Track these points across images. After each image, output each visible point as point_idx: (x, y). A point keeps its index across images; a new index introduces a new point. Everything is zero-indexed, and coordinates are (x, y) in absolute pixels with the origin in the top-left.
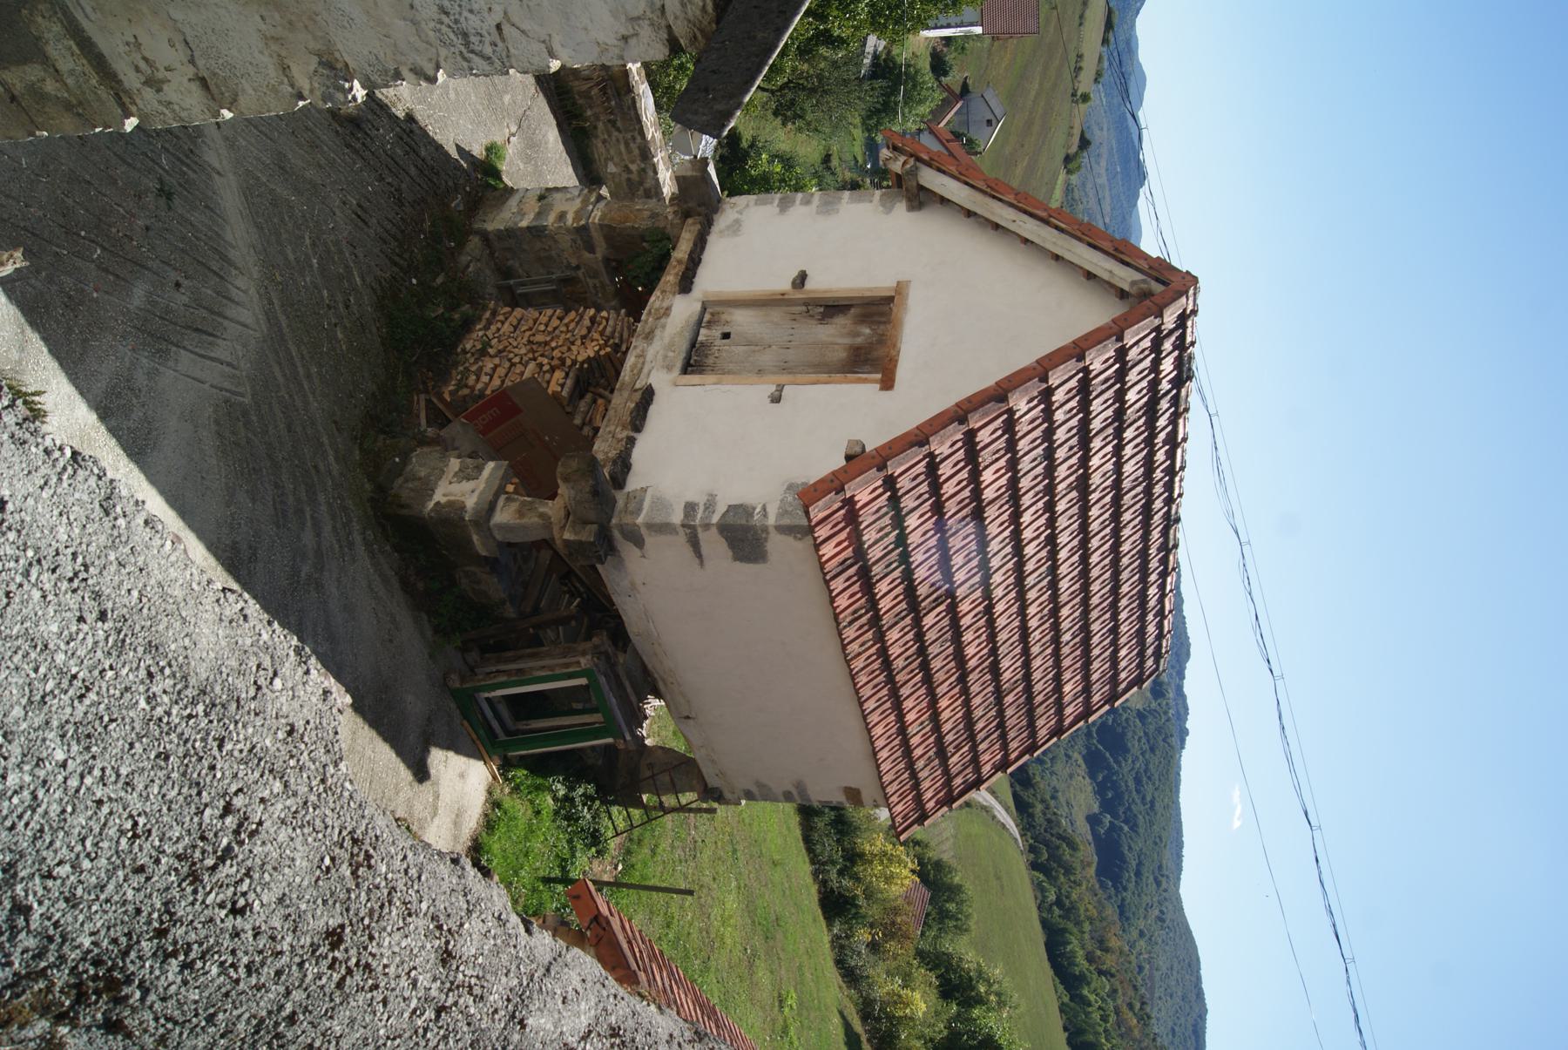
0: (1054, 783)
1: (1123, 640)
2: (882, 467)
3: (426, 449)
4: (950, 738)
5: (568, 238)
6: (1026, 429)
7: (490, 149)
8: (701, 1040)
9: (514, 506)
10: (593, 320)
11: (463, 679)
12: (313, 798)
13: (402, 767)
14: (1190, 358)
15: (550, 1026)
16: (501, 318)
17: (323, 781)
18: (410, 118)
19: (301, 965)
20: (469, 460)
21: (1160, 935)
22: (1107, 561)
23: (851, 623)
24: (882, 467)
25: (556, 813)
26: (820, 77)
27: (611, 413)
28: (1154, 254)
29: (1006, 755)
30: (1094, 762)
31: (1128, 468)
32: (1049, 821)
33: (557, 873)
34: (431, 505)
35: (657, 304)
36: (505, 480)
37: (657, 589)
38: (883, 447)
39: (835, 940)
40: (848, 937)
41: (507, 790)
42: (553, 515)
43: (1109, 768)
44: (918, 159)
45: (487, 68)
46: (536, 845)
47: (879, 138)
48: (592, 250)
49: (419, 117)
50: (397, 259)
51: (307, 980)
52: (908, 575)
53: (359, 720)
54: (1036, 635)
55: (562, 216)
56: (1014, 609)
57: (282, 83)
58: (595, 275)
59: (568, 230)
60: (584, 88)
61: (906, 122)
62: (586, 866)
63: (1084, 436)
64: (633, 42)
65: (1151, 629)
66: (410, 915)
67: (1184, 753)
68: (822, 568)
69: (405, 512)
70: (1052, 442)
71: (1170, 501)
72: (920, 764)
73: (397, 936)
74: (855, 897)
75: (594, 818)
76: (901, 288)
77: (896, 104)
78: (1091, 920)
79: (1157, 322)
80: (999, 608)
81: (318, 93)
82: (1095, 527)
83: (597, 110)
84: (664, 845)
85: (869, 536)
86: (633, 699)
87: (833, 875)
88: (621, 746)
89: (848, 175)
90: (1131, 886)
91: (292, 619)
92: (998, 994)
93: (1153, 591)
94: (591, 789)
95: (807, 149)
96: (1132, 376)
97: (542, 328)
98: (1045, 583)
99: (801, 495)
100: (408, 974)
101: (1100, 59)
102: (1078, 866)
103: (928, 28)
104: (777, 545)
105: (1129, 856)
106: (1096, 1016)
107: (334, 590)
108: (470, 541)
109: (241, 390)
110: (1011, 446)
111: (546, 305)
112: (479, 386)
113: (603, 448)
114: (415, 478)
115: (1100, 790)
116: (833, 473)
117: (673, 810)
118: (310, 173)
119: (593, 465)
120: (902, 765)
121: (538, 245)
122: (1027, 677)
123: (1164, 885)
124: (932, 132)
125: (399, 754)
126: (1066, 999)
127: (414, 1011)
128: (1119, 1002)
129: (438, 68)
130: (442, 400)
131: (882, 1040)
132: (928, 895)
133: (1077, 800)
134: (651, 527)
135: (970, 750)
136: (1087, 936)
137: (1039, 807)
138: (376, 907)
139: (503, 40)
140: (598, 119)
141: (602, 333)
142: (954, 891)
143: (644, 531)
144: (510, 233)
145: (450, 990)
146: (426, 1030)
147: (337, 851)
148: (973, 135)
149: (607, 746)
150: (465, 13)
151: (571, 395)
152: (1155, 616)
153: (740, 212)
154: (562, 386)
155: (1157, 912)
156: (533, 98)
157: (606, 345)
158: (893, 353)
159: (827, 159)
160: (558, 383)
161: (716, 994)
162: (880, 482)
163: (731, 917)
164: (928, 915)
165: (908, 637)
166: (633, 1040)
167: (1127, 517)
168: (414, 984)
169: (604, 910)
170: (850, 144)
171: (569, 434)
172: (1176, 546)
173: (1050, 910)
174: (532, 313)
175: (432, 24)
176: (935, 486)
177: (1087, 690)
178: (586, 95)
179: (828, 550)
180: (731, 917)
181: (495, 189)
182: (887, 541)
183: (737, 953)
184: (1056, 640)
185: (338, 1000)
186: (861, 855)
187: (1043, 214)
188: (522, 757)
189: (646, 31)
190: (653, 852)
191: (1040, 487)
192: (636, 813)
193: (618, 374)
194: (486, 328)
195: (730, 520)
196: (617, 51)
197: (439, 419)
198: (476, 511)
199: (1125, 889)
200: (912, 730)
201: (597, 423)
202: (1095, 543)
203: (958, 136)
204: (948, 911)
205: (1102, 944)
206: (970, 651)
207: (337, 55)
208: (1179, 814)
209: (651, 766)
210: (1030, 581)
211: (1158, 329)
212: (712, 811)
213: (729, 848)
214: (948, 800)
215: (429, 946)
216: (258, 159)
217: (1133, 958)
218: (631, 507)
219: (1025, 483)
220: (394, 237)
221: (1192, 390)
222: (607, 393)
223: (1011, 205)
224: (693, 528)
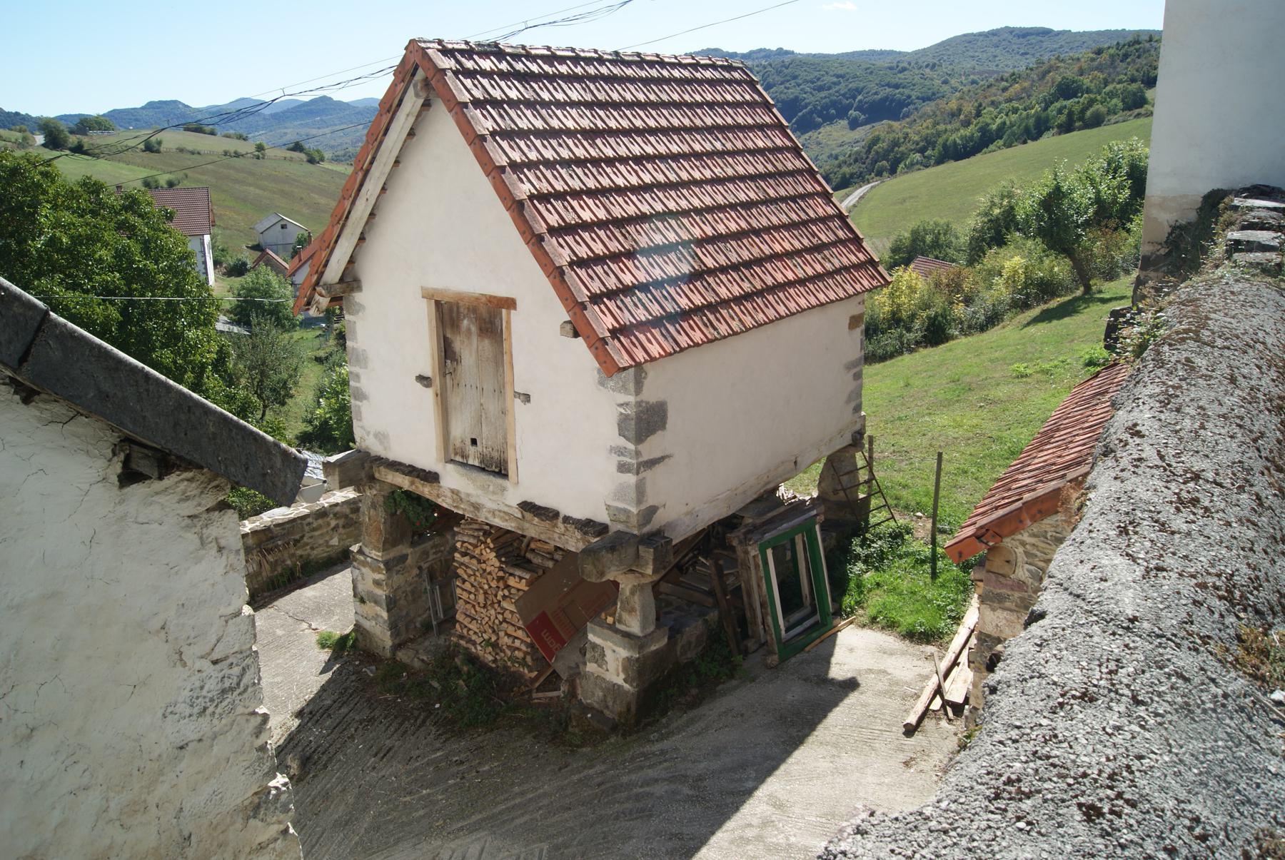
0: (824, 157)
1: (719, 98)
2: (583, 306)
3: (579, 691)
4: (806, 242)
5: (395, 578)
6: (545, 184)
7: (323, 646)
8: (1112, 451)
9: (625, 616)
10: (464, 554)
11: (771, 653)
12: (964, 842)
13: (847, 701)
14: (479, 45)
15: (1130, 593)
16: (465, 631)
17: (945, 832)
18: (299, 714)
19: (1123, 847)
20: (588, 656)
21: (946, 68)
22: (653, 113)
23: (715, 329)
24: (583, 306)
25: (877, 569)
26: (251, 368)
27: (543, 537)
28: (391, 78)
29: (818, 194)
30: (805, 125)
31: (575, 96)
32: (856, 160)
33: (927, 567)
34: (627, 686)
35: (449, 501)
36: (603, 625)
37: (690, 494)
38: (566, 306)
39: (965, 333)
40: (961, 323)
41: (861, 612)
42: (632, 584)
43: (811, 112)
44: (317, 283)
45: (252, 670)
46: (905, 585)
47: (300, 317)
48: (403, 558)
49: (299, 707)
50: (419, 722)
51: (1136, 839)
52: (673, 281)
53: (811, 739)
54: (718, 171)
55: (377, 583)
56: (697, 190)
57: (274, 849)
58: (425, 553)
59: (388, 578)
60: (267, 566)
61: (285, 294)
62: (919, 544)
63: (548, 134)
64: (223, 543)
65: (708, 74)
66: (1056, 736)
67: (797, 51)
68: (670, 354)
69: (633, 709)
70: (555, 162)
71: (601, 61)
72: (829, 266)
73: (1078, 748)
74: (929, 317)
75: (880, 539)
76: (428, 295)
77: (271, 304)
78: (936, 124)
79: (449, 74)
80: (696, 203)
81: (282, 816)
82: (625, 124)
83: (286, 555)
84: (898, 477)
85: (642, 315)
86: (782, 509)
87: (911, 336)
88: (822, 518)
89: (332, 342)
90: (907, 92)
91: (729, 800)
92: (1002, 197)
93: (676, 73)
94: (856, 541)
95: (311, 377)
96: (497, 94)
97: (472, 596)
98: (673, 165)
99: (610, 376)
100: (1110, 735)
101: (227, 136)
102: (891, 136)
103: (207, 279)
104: (651, 393)
105: (882, 95)
106: (1014, 117)
107: (702, 765)
108: (656, 652)
109: (537, 853)
110: (560, 196)
111: (453, 594)
112: (524, 648)
113: (574, 542)
114: (604, 700)
115: (829, 119)
116: (590, 347)
117: (871, 471)
118: (350, 799)
119: (589, 552)
120: (830, 281)
121: (402, 602)
122: (753, 178)
123: (905, 65)
124: (293, 274)
125: (836, 705)
126: (1001, 142)
127: (1142, 727)
128: (1001, 99)
129: (254, 713)
130: (537, 678)
131: (1044, 292)
132: (921, 258)
133: (838, 138)
134: (639, 501)
135: (815, 224)
136: (949, 127)
137: (845, 169)
138: (1055, 771)
139: (226, 658)
140: (293, 555)
141: (475, 546)
142: (917, 236)
143: (643, 507)
144: (393, 626)
145: (1116, 692)
146: (1157, 715)
147: (1010, 815)
148: (294, 240)
149: (822, 530)
150: (204, 692)
151: (529, 570)
152: (697, 71)
153: (368, 433)
154: (521, 578)
155: (928, 70)
156: (278, 610)
157: (485, 543)
158: (484, 299)
159: (319, 360)
160: (520, 582)
161: (1019, 430)
162: (596, 307)
163: (954, 420)
164: (937, 257)
165: (725, 280)
166: (1127, 513)
167: (615, 97)
168: (1118, 728)
169: (969, 531)
170: (306, 341)
171: (559, 573)
172: (638, 55)
173: (928, 158)
174: (460, 605)
175: (215, 722)
176: (598, 260)
177: (761, 127)
178: (274, 565)
179: (655, 350)
180: (954, 420)
181: (356, 640)
182: (645, 300)
183: (984, 413)
184: (722, 154)
185: (1148, 806)
186: (894, 313)
187: (360, 175)
188: (833, 600)
189: (213, 531)
190: (905, 487)
191: (594, 170)
192: (874, 502)
193: (508, 532)
194: (474, 643)
195: (632, 434)
196: (232, 556)
197: (553, 681)
198: (631, 648)
199: (909, 97)
200: (801, 274)
201: (551, 547)
202: (639, 123)
203: (295, 253)
204: (933, 241)
205: (954, 115)
206: (733, 227)
207: (246, 803)
208: (847, 54)
209: (835, 492)
210: (673, 177)
211: (456, 73)
212: (871, 440)
213: (898, 423)
214: (857, 241)
215: (1081, 716)
216: (340, 844)
217: (965, 89)
218: (623, 518)
219: (591, 184)
220: (401, 724)
221: (510, 43)
222: (526, 541)
223: (353, 203)
224: (639, 465)
